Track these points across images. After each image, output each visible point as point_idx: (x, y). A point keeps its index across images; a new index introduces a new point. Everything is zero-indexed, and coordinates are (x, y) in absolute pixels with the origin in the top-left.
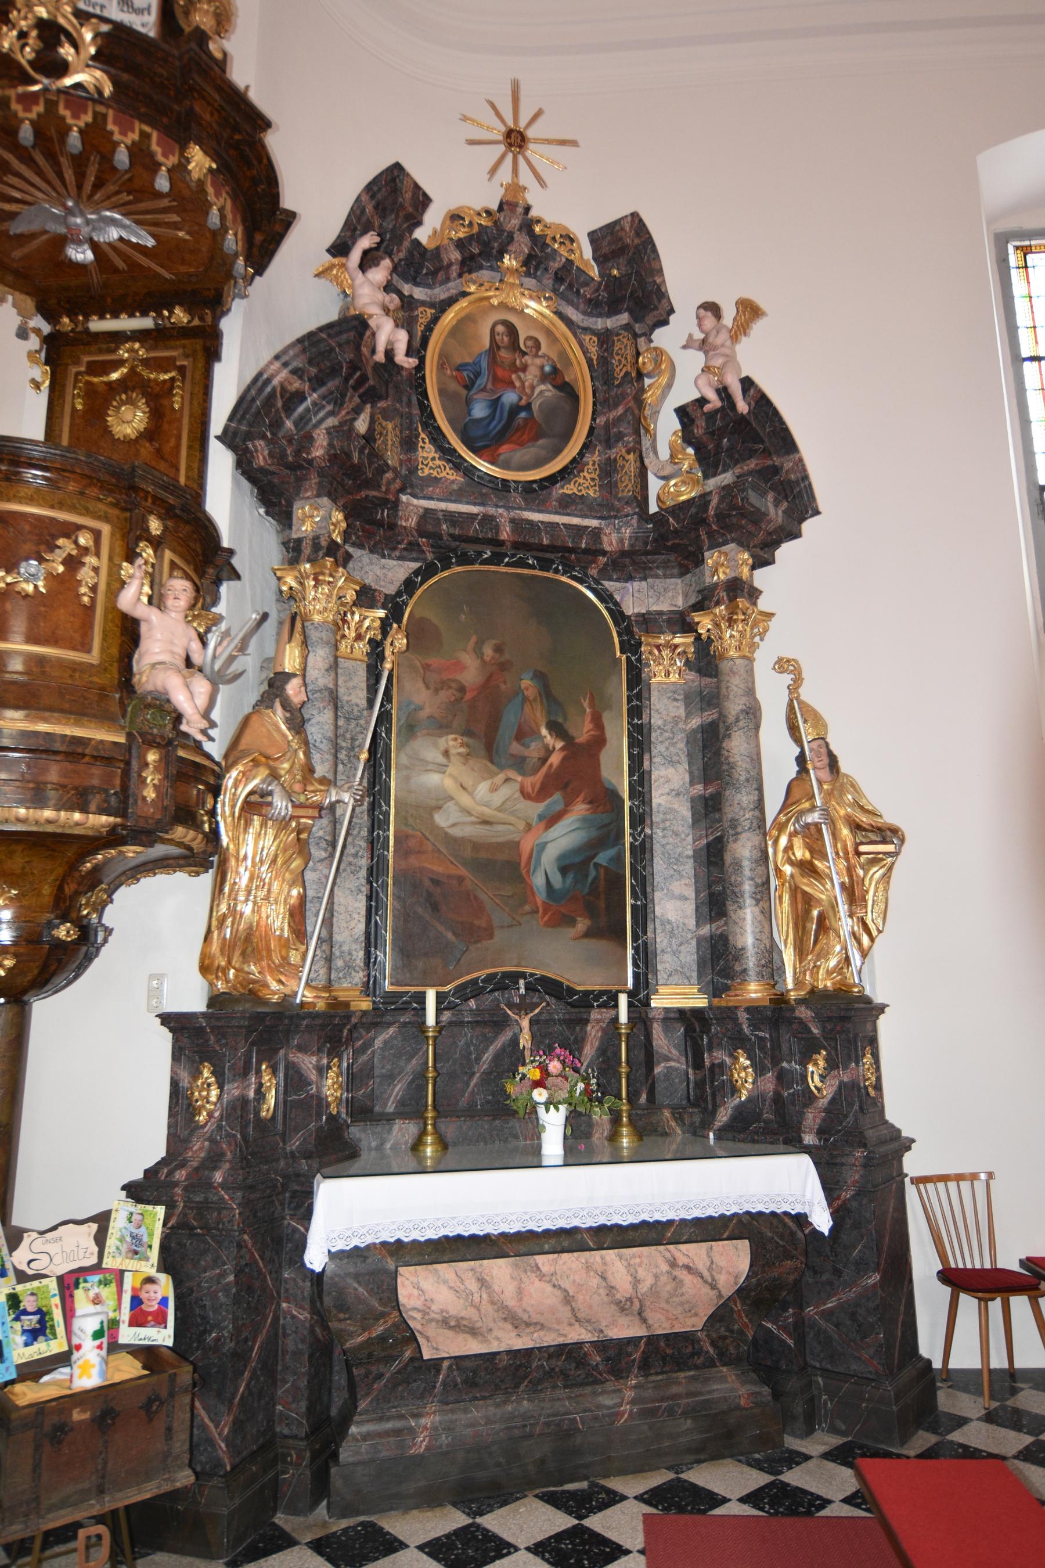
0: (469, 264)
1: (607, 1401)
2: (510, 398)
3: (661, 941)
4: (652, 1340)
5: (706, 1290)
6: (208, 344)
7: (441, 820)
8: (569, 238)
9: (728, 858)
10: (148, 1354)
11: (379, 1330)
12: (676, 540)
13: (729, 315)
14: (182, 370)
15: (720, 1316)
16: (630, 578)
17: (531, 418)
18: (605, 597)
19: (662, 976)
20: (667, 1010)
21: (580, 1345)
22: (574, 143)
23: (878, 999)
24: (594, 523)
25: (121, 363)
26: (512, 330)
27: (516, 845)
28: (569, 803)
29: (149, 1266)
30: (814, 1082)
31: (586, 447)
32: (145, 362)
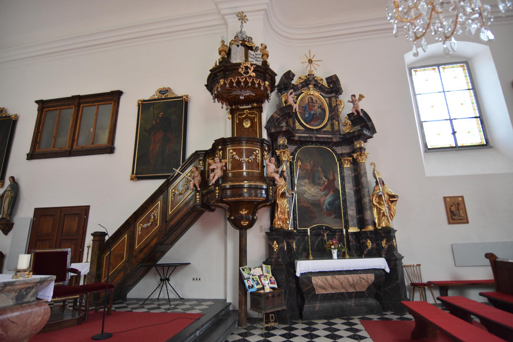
0: (303, 87)
1: (349, 303)
2: (312, 112)
3: (349, 219)
4: (356, 292)
5: (366, 283)
6: (261, 110)
7: (305, 196)
8: (322, 80)
9: (363, 202)
10: (273, 288)
11: (309, 288)
12: (349, 140)
13: (357, 97)
14: (256, 114)
15: (369, 288)
16: (338, 146)
17: (317, 116)
18: (333, 150)
19: (350, 225)
20: (352, 232)
21: (343, 293)
22: (321, 61)
23: (395, 229)
24: (330, 136)
25: (245, 114)
26: (312, 99)
27: (319, 200)
28: (329, 192)
29: (270, 275)
30: (384, 245)
31: (328, 121)
32: (249, 113)
